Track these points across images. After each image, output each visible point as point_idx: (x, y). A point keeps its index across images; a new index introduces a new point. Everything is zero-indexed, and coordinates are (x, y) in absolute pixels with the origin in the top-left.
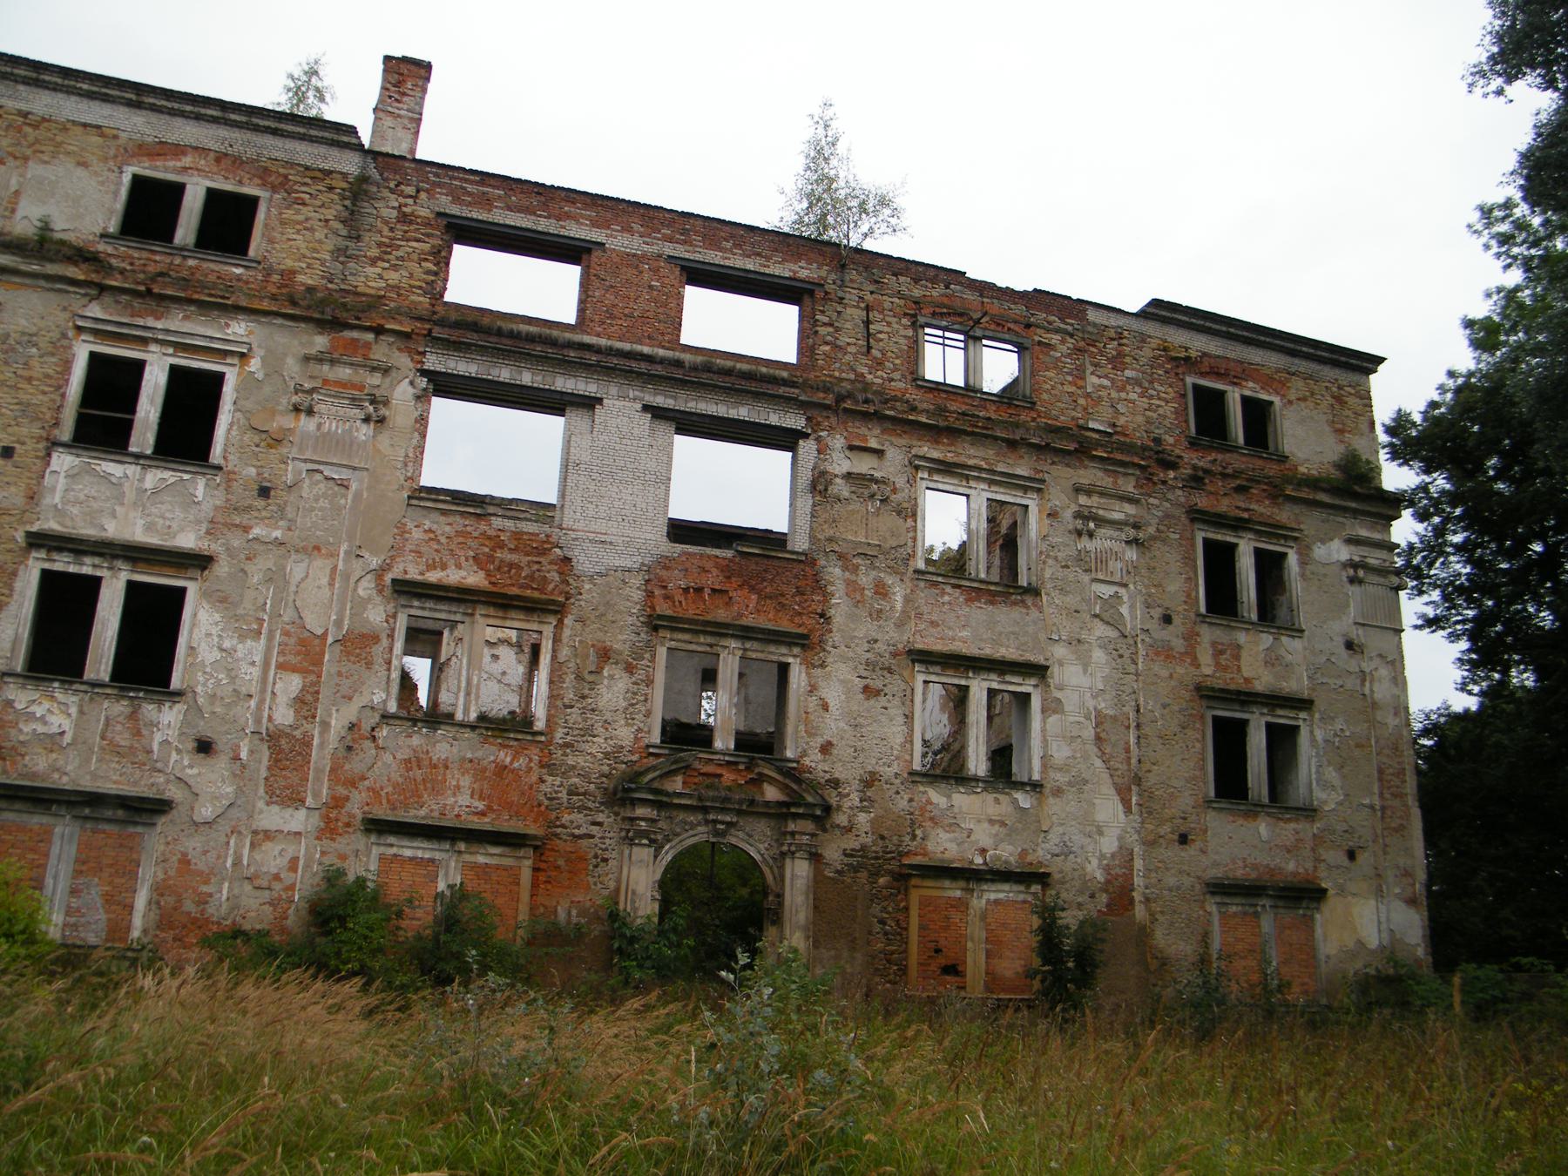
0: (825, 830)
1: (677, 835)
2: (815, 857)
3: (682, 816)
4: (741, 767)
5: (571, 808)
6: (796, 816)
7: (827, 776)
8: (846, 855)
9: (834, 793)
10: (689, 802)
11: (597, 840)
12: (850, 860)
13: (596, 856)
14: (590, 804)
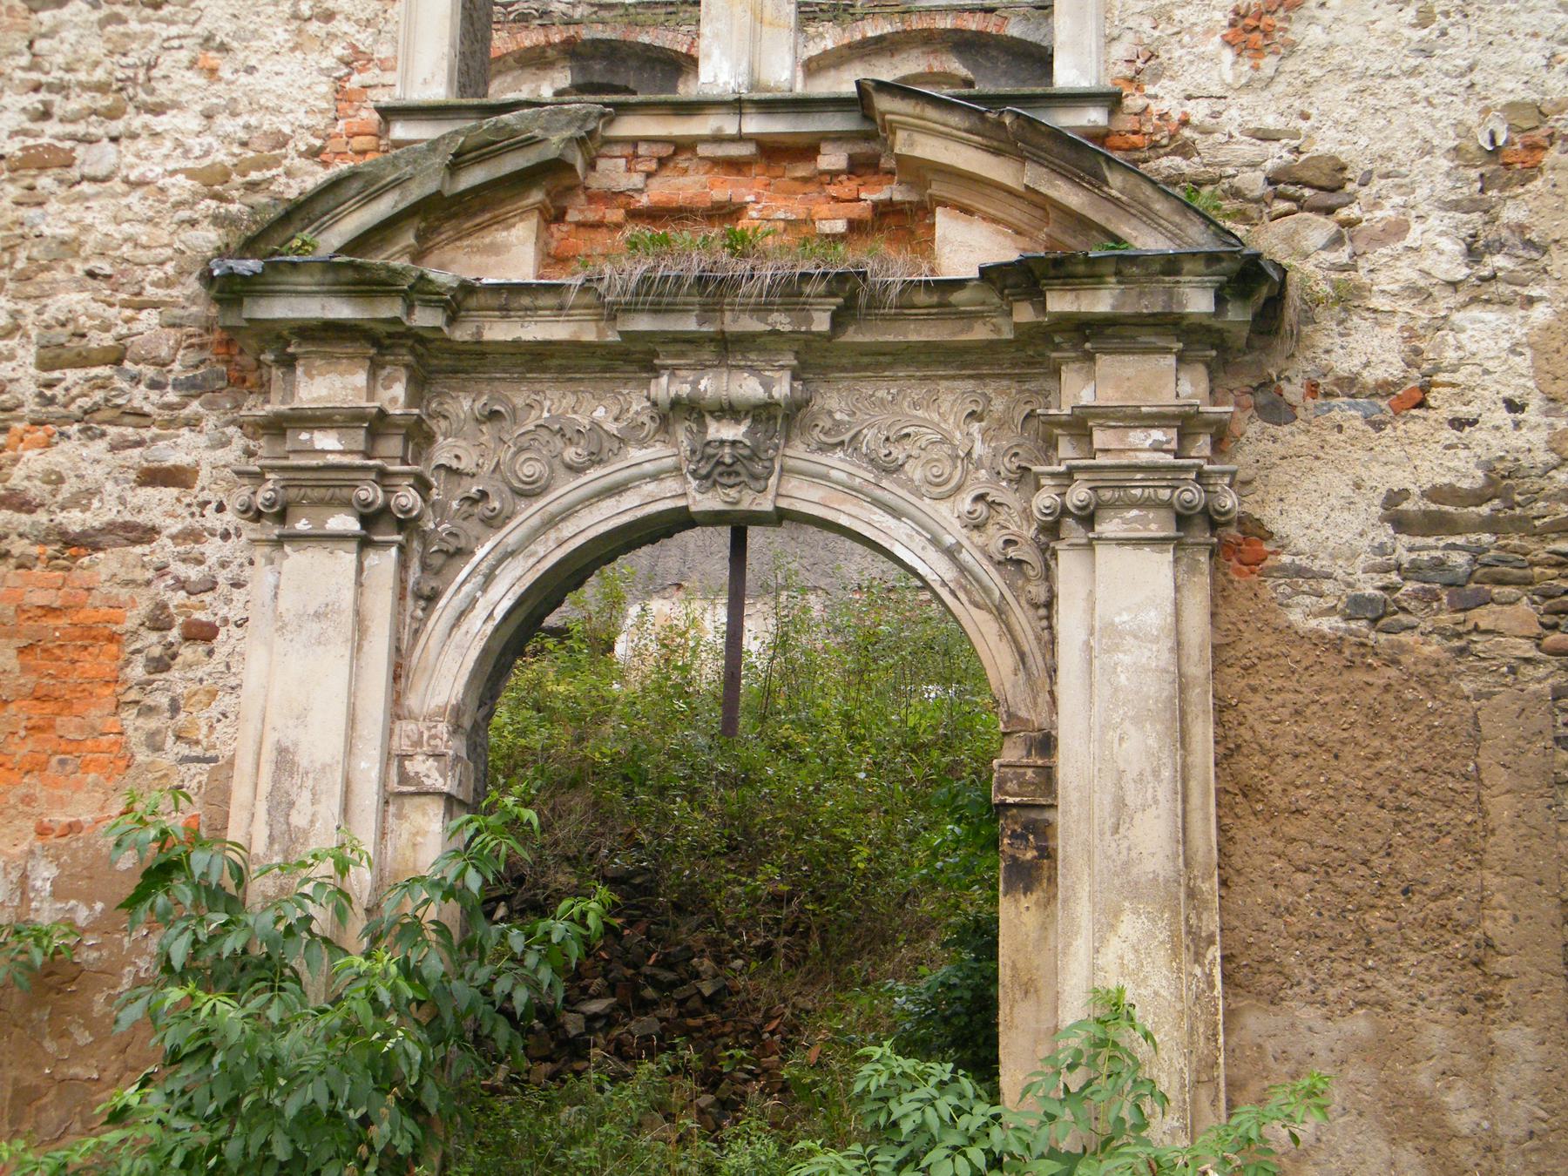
0: (1277, 411)
1: (529, 492)
2: (1222, 541)
3: (553, 402)
4: (832, 159)
5: (51, 421)
6: (1091, 335)
7: (1276, 155)
8: (1401, 523)
9: (1318, 230)
10: (558, 331)
11: (163, 550)
12: (1431, 547)
13: (159, 621)
14: (140, 397)
